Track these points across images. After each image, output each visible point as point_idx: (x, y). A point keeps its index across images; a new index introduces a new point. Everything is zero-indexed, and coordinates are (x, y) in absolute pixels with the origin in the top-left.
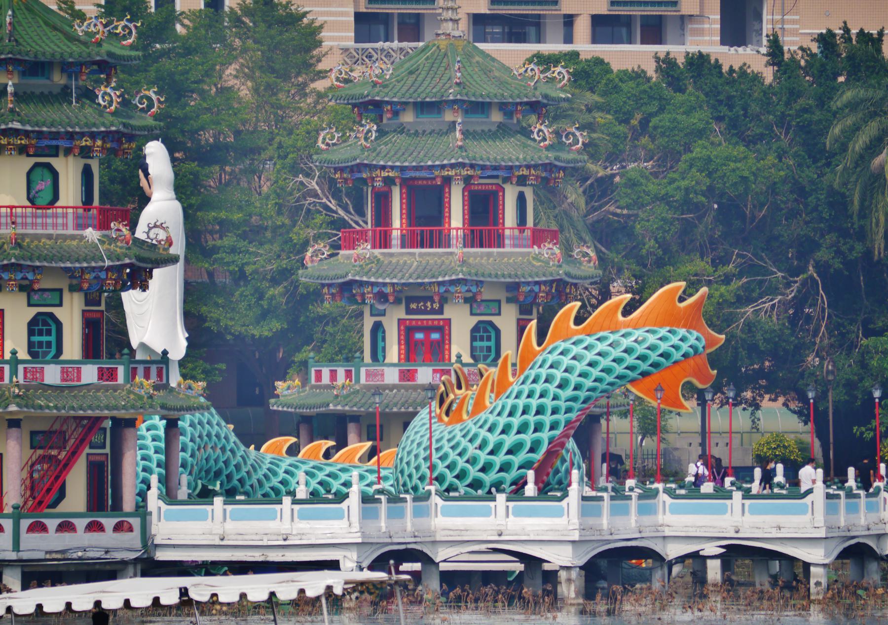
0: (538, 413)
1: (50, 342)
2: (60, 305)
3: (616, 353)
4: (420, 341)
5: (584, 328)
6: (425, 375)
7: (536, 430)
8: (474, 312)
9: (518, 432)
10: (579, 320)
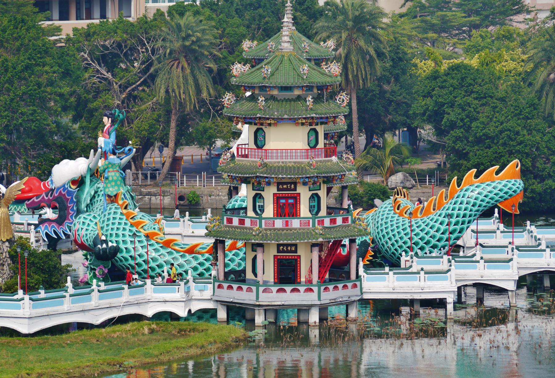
0: (463, 217)
2: (320, 189)
3: (496, 191)
5: (479, 180)
7: (462, 224)
9: (455, 225)
10: (477, 176)
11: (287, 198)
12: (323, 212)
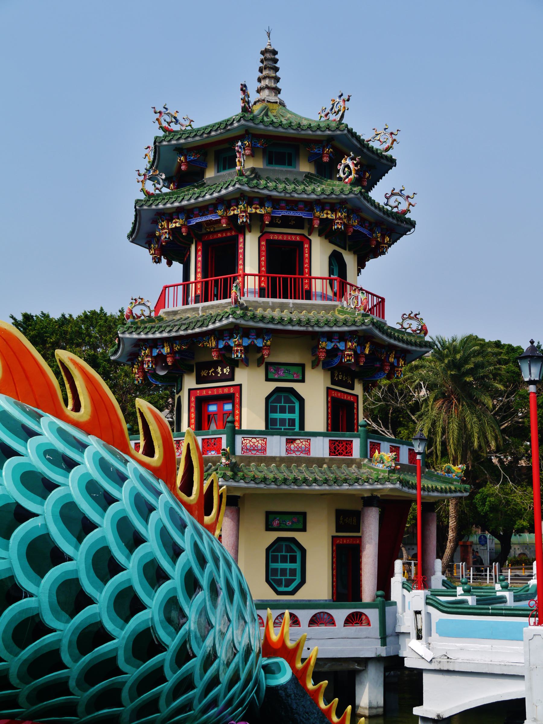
1: (295, 570)
4: (214, 414)
8: (271, 376)
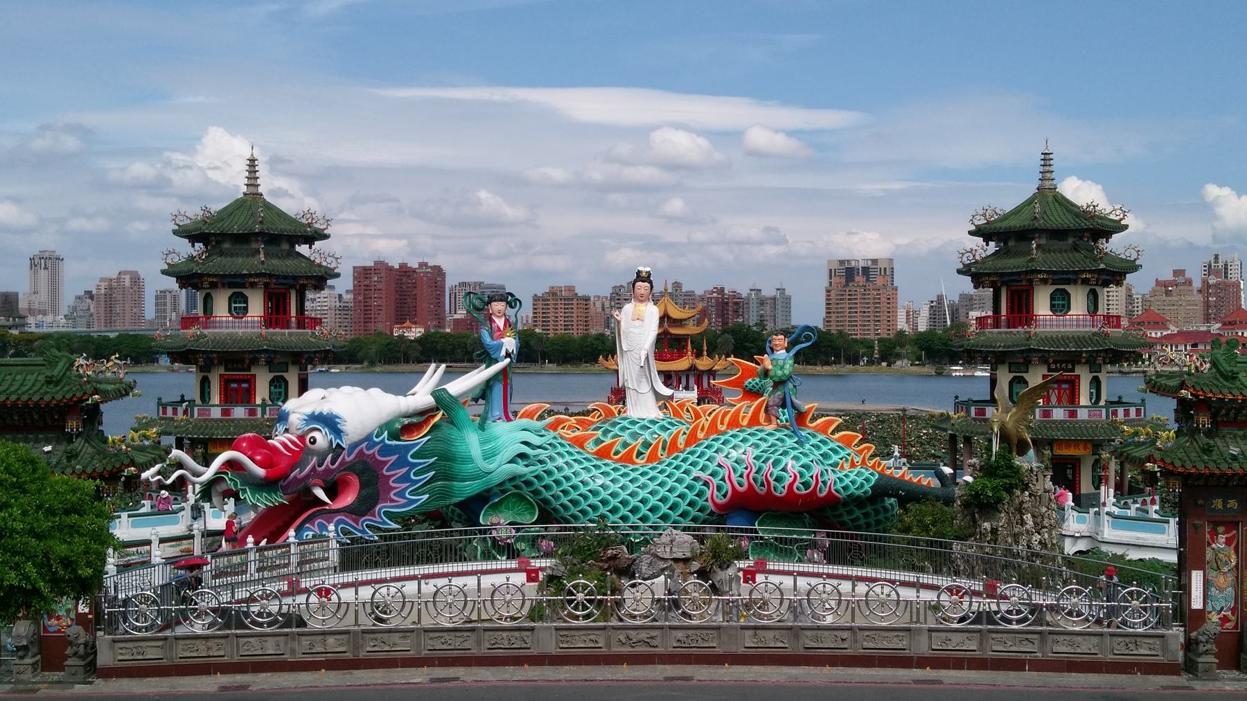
6: (239, 412)
11: (239, 381)
12: (1102, 403)
